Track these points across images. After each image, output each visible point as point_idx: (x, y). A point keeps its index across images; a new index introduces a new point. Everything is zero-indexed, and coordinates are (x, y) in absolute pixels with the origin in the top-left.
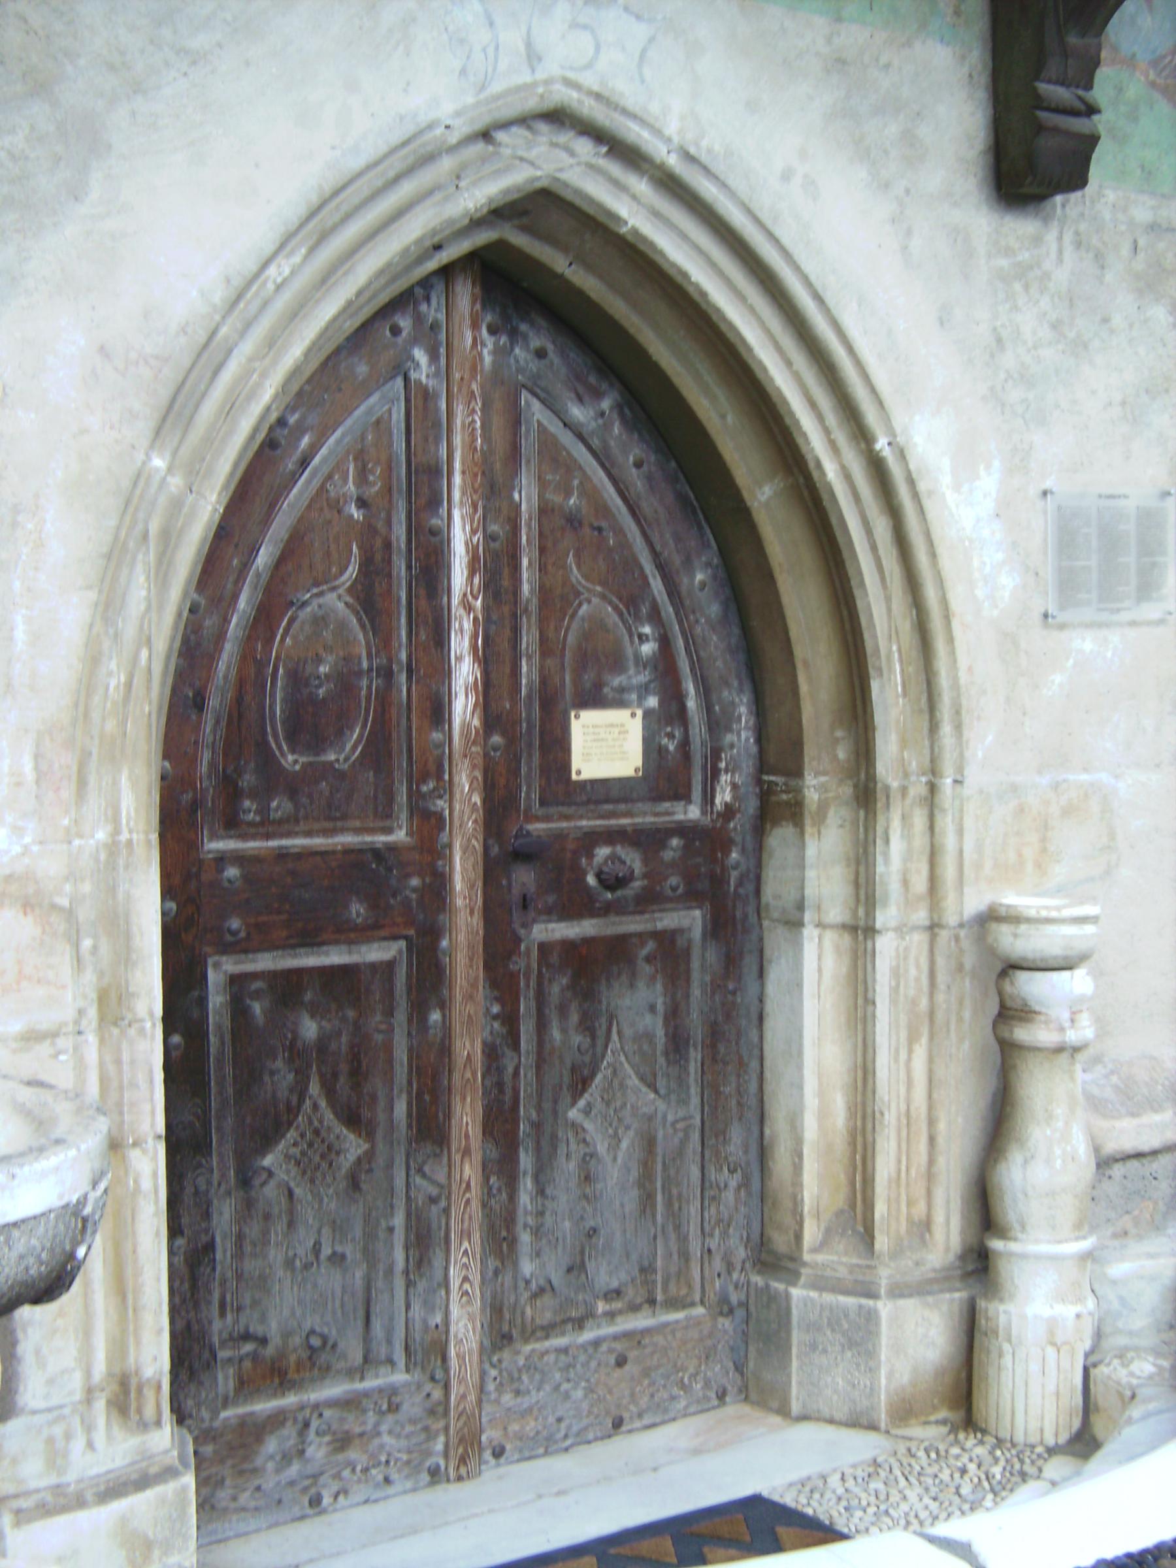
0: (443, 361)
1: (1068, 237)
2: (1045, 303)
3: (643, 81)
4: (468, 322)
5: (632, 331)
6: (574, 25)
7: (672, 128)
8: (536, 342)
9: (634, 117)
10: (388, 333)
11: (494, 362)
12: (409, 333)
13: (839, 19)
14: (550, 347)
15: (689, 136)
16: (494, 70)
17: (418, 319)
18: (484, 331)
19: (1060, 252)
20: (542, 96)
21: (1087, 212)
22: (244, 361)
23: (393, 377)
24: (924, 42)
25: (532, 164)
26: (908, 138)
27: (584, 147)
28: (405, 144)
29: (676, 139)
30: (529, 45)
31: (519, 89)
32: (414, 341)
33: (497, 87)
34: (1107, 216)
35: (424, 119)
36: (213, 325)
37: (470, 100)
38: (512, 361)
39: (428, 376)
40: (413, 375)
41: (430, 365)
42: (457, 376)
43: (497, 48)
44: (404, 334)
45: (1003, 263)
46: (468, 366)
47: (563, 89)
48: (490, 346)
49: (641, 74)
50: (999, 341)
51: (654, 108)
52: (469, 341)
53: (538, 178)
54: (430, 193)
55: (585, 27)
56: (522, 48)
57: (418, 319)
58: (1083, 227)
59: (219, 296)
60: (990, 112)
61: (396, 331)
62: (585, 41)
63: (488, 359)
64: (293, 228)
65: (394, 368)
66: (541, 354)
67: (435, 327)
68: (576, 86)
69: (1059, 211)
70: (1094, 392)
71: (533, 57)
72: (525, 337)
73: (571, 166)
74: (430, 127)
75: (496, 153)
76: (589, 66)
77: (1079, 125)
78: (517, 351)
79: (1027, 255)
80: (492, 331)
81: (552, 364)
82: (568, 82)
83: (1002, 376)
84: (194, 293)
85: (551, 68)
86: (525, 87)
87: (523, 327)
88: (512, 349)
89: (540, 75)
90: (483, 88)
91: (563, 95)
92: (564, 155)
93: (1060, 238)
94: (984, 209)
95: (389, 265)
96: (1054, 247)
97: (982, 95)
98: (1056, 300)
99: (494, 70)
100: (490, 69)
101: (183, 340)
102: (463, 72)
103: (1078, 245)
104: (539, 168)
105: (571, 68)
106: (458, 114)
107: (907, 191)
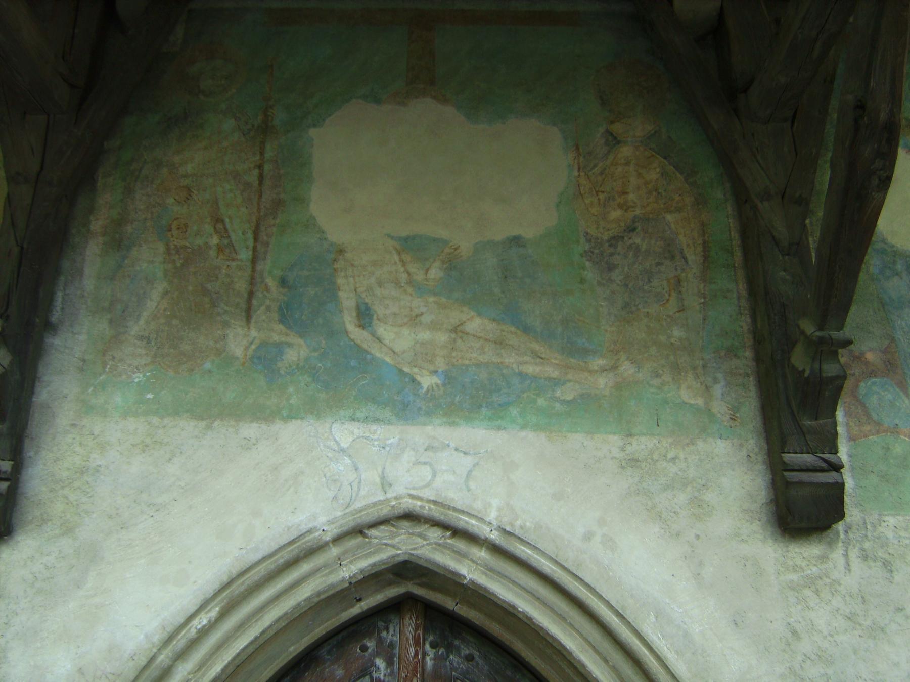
0: (396, 666)
1: (854, 553)
2: (837, 602)
3: (469, 490)
4: (412, 641)
5: (508, 643)
6: (417, 463)
7: (492, 516)
8: (465, 651)
9: (463, 512)
10: (358, 650)
11: (434, 665)
12: (373, 650)
13: (631, 435)
14: (476, 654)
15: (505, 520)
16: (357, 495)
17: (380, 641)
18: (427, 647)
19: (848, 564)
20: (393, 507)
21: (869, 534)
22: (185, 674)
23: (364, 676)
24: (704, 441)
25: (393, 546)
26: (696, 502)
27: (435, 534)
28: (291, 543)
29: (495, 523)
30: (383, 478)
31: (375, 504)
32: (377, 654)
33: (358, 505)
34: (890, 535)
35: (304, 528)
36: (152, 654)
37: (339, 514)
38: (448, 663)
39: (385, 675)
40: (375, 675)
41: (387, 668)
42: (403, 675)
43: (360, 483)
44: (370, 650)
45: (794, 577)
46: (411, 668)
47: (410, 501)
48: (432, 655)
49: (467, 486)
50: (795, 633)
51: (478, 505)
52: (413, 653)
53: (398, 555)
54: (325, 566)
55: (425, 463)
56: (378, 480)
57: (380, 641)
58: (867, 545)
59: (157, 638)
60: (769, 477)
61: (364, 649)
62: (426, 472)
63: (429, 663)
64: (208, 596)
65: (362, 671)
66: (469, 658)
67: (392, 645)
68: (420, 498)
69: (842, 536)
70: (896, 664)
71: (385, 484)
72: (458, 649)
73: (423, 546)
74: (310, 531)
75: (369, 542)
76: (428, 485)
77: (830, 477)
78: (451, 657)
79: (814, 569)
80: (433, 646)
81: (478, 664)
82: (412, 496)
83: (800, 658)
84: (142, 636)
85: (399, 489)
86: (381, 502)
87: (457, 642)
88: (448, 657)
89: (389, 495)
90: (348, 506)
91: (408, 504)
92: (419, 540)
93: (846, 555)
94: (770, 542)
95: (286, 614)
96: (841, 561)
97: (760, 467)
98: (848, 598)
99: (357, 495)
100: (354, 495)
101: (131, 664)
102: (335, 498)
103: (865, 557)
104: (399, 549)
105: (414, 488)
106: (330, 522)
107: (698, 537)
